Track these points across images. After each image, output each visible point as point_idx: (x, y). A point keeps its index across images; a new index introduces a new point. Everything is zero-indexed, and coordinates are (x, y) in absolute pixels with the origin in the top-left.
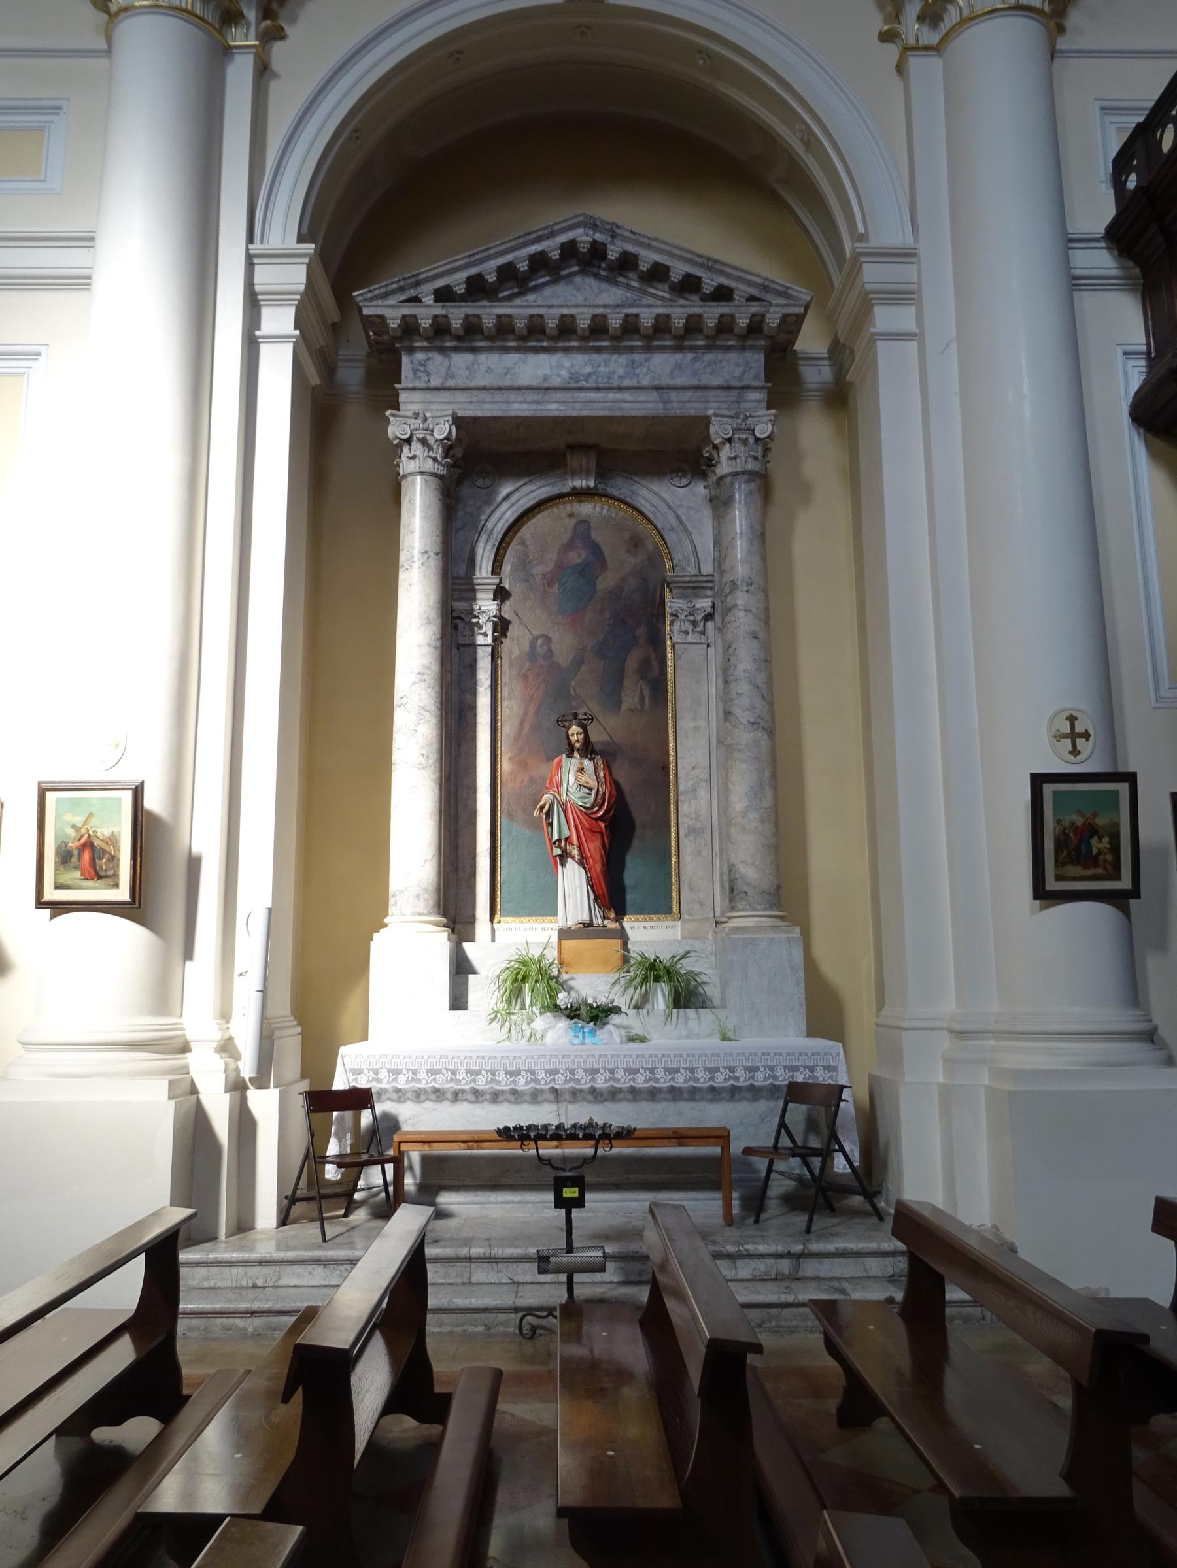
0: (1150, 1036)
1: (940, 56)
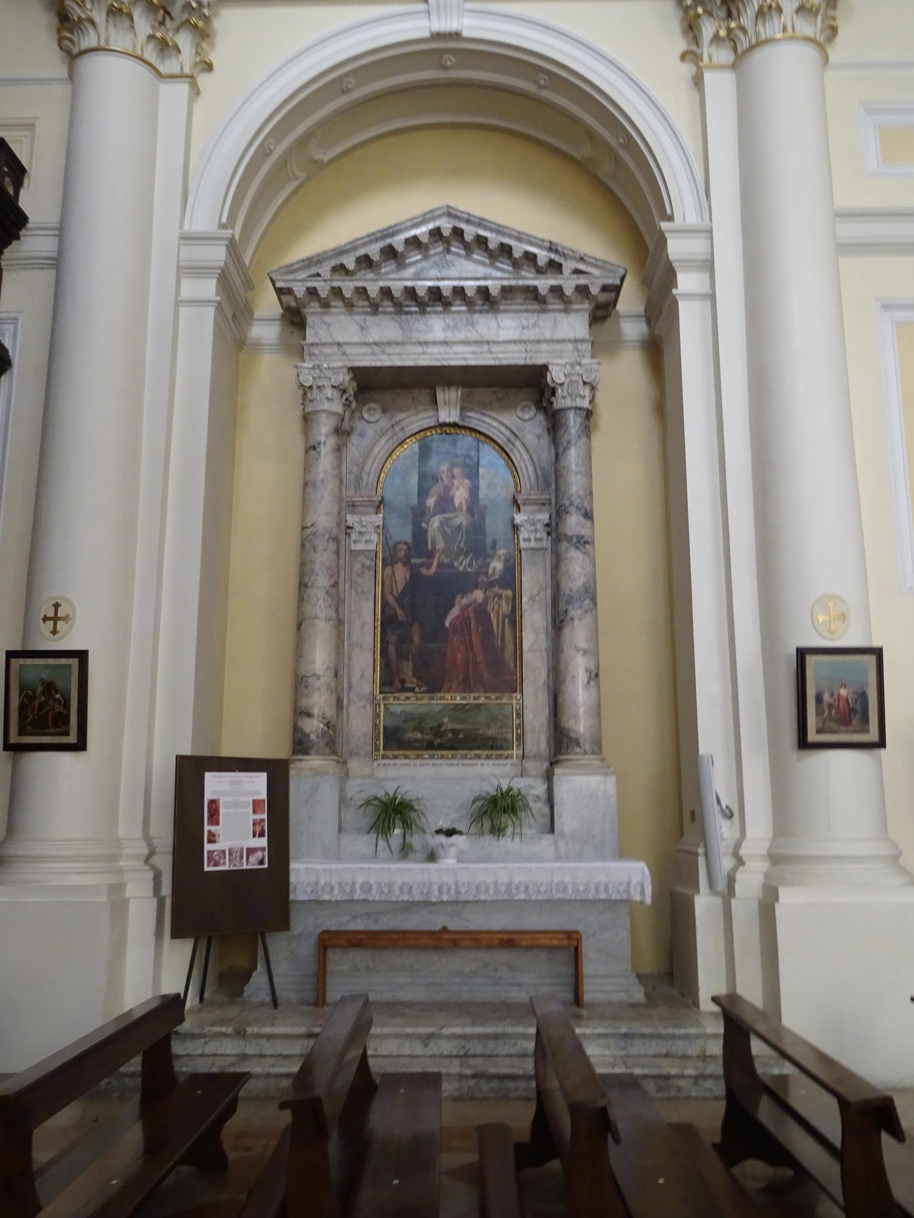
0: (895, 859)
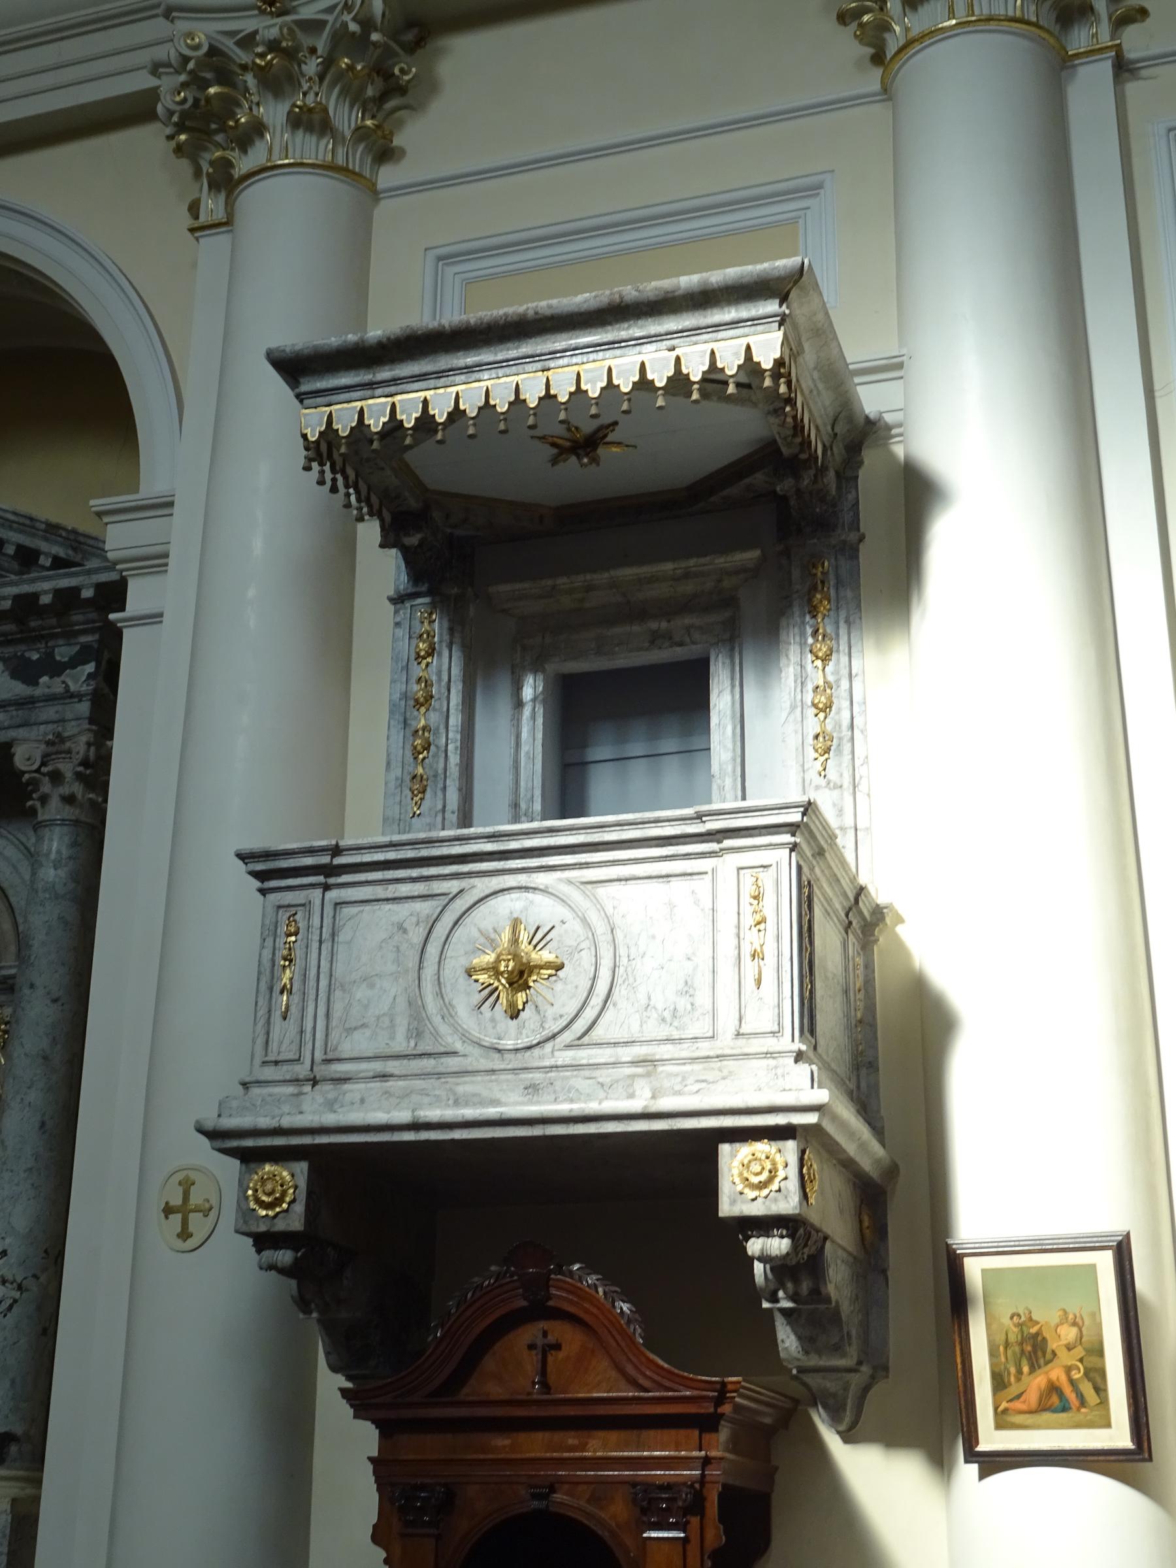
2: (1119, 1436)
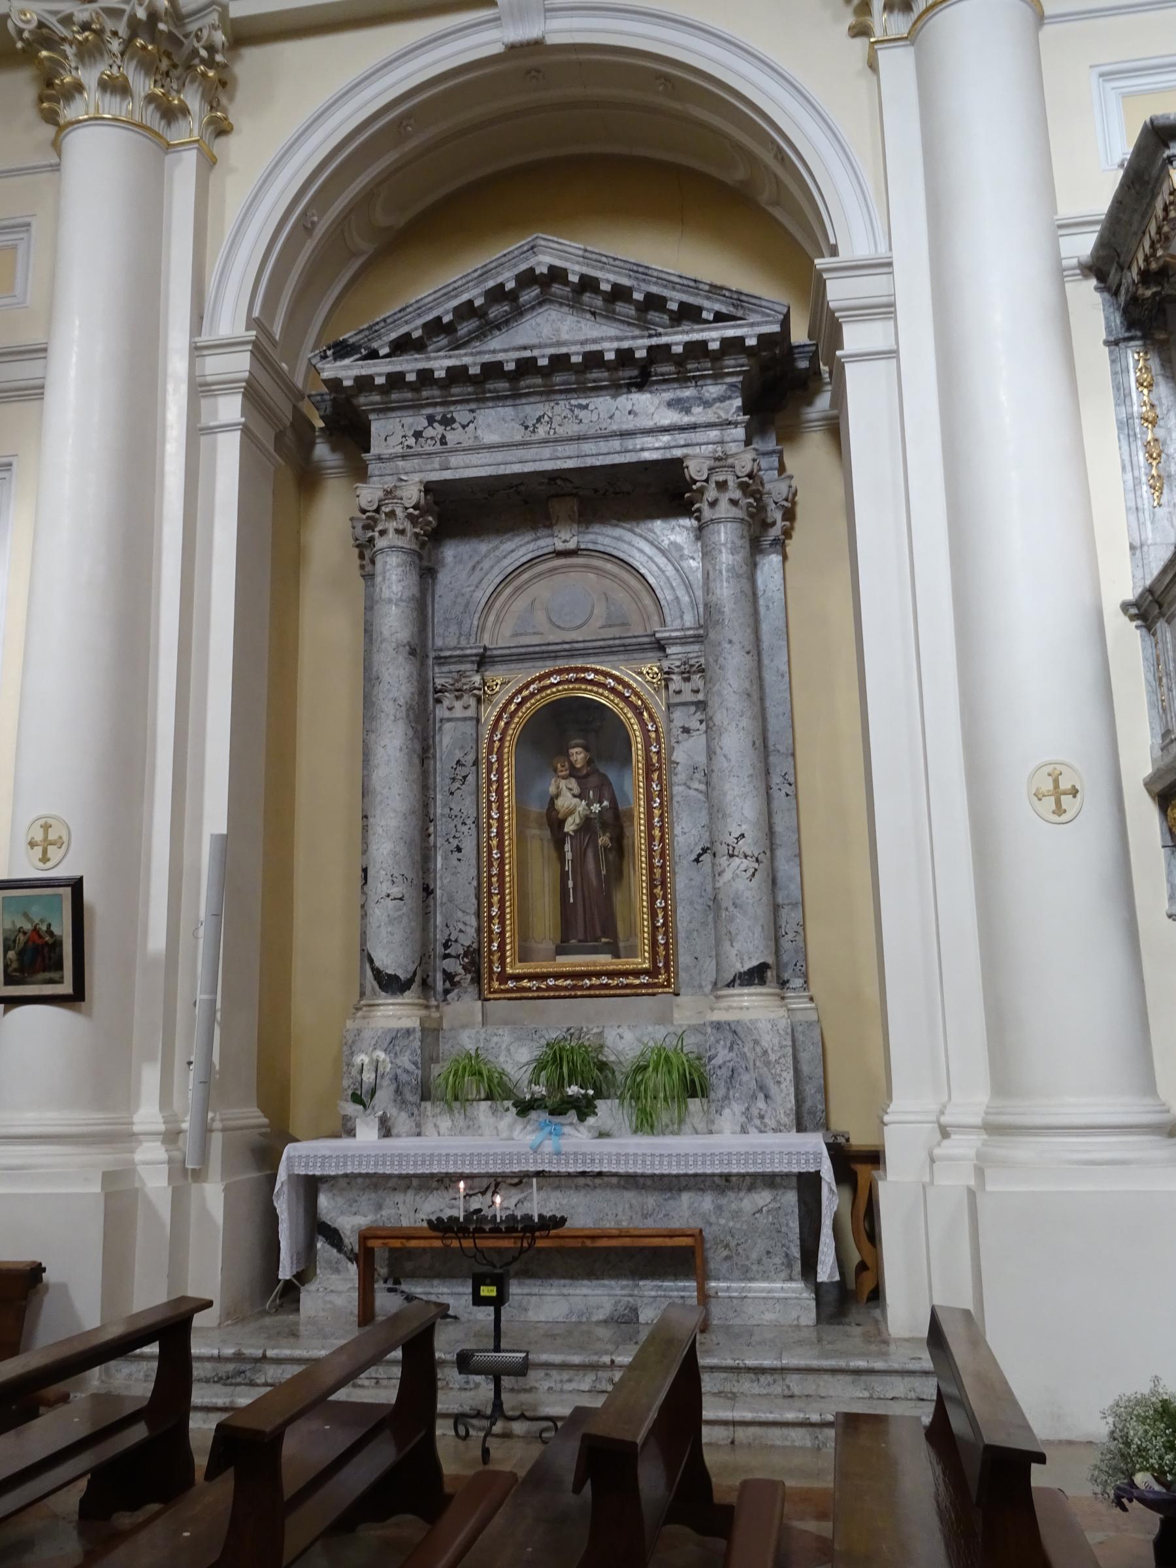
1: (912, 44)
2: (66, 988)
